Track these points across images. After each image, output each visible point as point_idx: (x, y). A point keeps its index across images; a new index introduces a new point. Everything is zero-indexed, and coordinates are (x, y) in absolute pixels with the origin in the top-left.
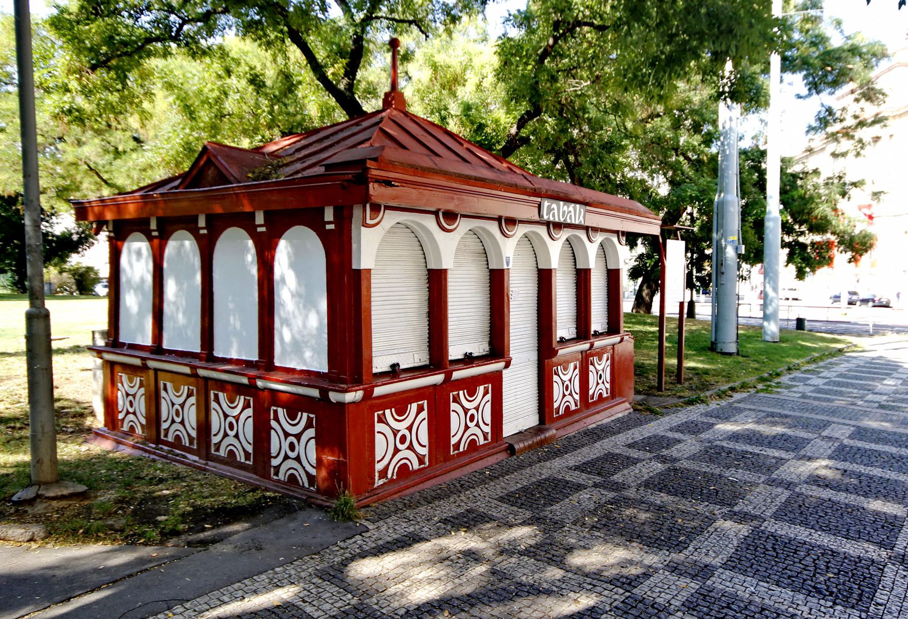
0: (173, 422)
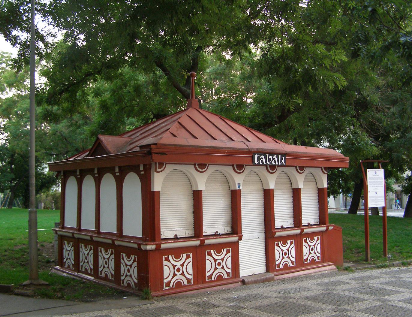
0: (84, 262)
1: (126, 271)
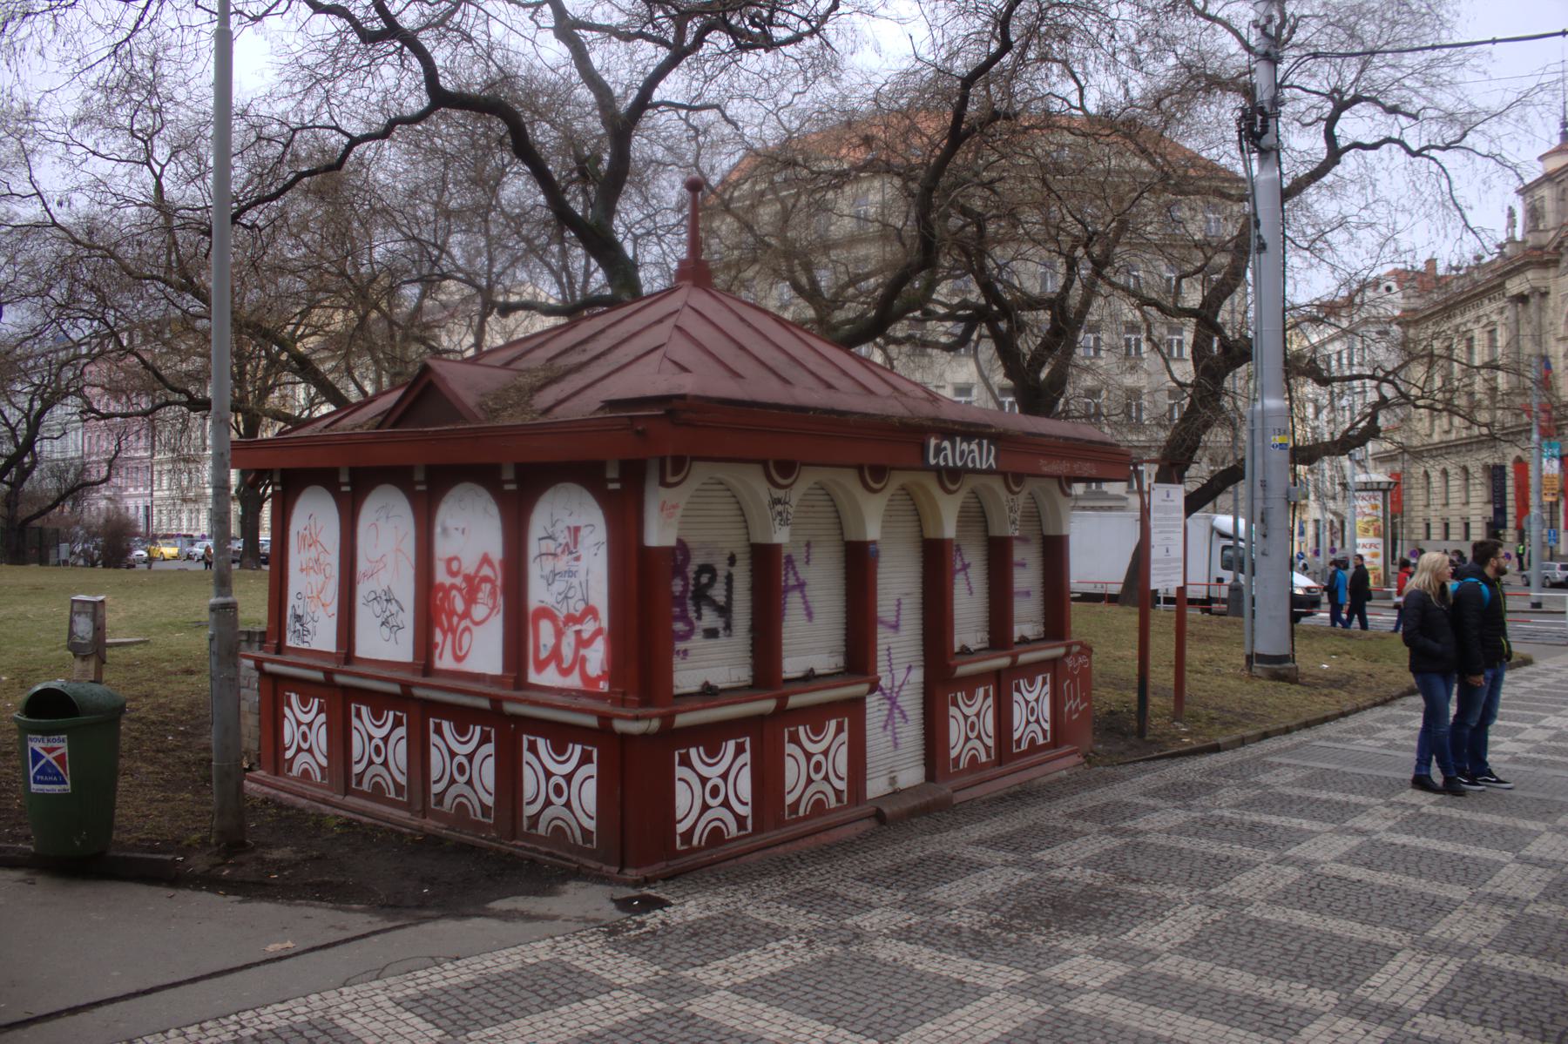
0: (371, 762)
1: (298, 736)
